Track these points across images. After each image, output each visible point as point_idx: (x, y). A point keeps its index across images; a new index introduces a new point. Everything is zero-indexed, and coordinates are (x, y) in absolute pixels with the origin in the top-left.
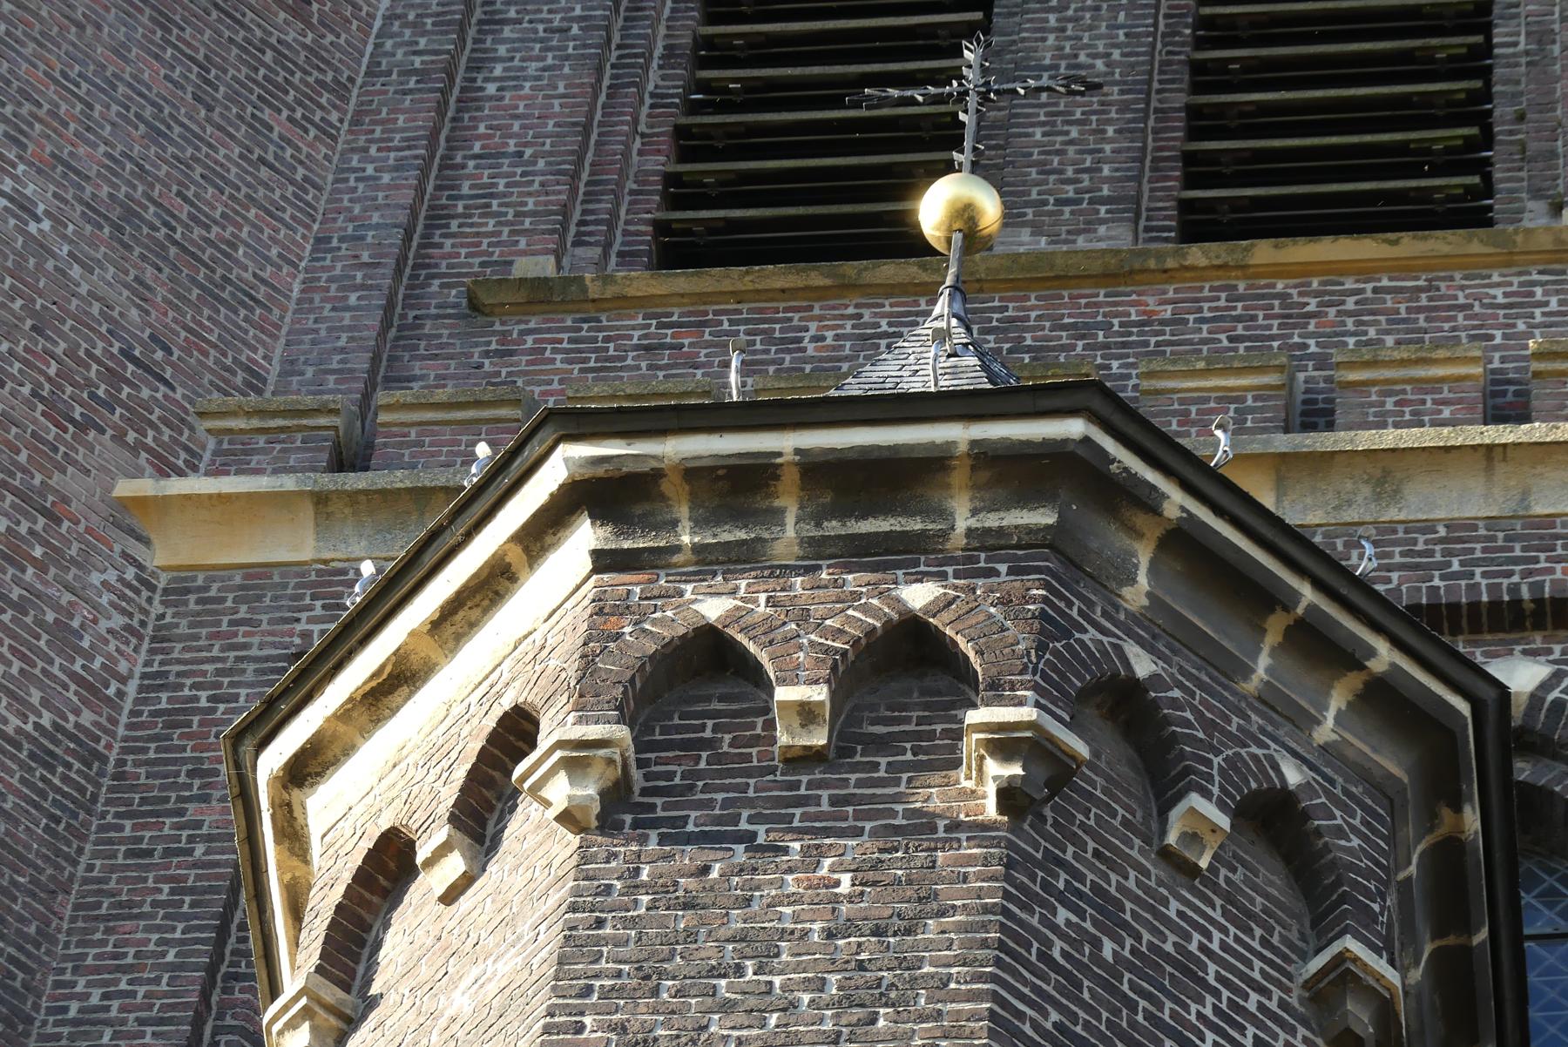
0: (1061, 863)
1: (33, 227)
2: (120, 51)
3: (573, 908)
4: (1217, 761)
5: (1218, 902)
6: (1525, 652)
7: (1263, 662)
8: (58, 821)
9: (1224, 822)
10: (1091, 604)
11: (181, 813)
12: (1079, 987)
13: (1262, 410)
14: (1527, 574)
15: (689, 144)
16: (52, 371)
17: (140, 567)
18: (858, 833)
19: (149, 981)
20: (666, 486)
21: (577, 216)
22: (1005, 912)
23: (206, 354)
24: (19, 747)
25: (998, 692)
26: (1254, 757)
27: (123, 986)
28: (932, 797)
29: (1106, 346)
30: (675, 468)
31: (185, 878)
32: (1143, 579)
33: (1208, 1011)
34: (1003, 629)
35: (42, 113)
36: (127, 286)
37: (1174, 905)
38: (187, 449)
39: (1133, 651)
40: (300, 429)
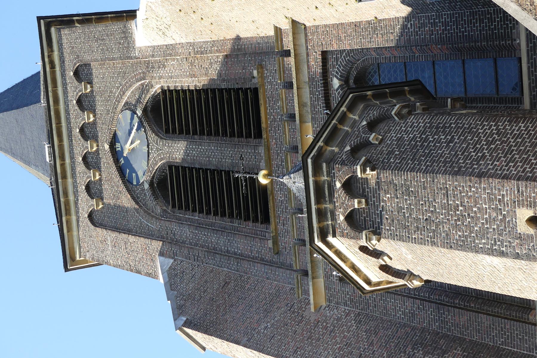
0: (383, 160)
1: (269, 326)
2: (238, 313)
3: (394, 239)
4: (363, 135)
5: (387, 135)
6: (332, 82)
7: (346, 128)
8: (370, 320)
9: (374, 134)
10: (338, 157)
11: (368, 299)
12: (404, 157)
13: (291, 125)
14: (318, 82)
15: (247, 219)
16: (294, 323)
17: (326, 307)
18: (379, 194)
19: (397, 304)
20: (321, 226)
21: (261, 237)
22: (392, 170)
23: (288, 297)
24: (358, 326)
25: (355, 172)
26: (362, 129)
27: (398, 308)
28: (373, 183)
29: (280, 150)
30: (318, 225)
31: (379, 299)
32: (333, 149)
33: (406, 136)
34: (344, 171)
35: (249, 325)
36: (278, 310)
37: (388, 142)
38: (305, 300)
39: (346, 150)
40: (301, 281)
